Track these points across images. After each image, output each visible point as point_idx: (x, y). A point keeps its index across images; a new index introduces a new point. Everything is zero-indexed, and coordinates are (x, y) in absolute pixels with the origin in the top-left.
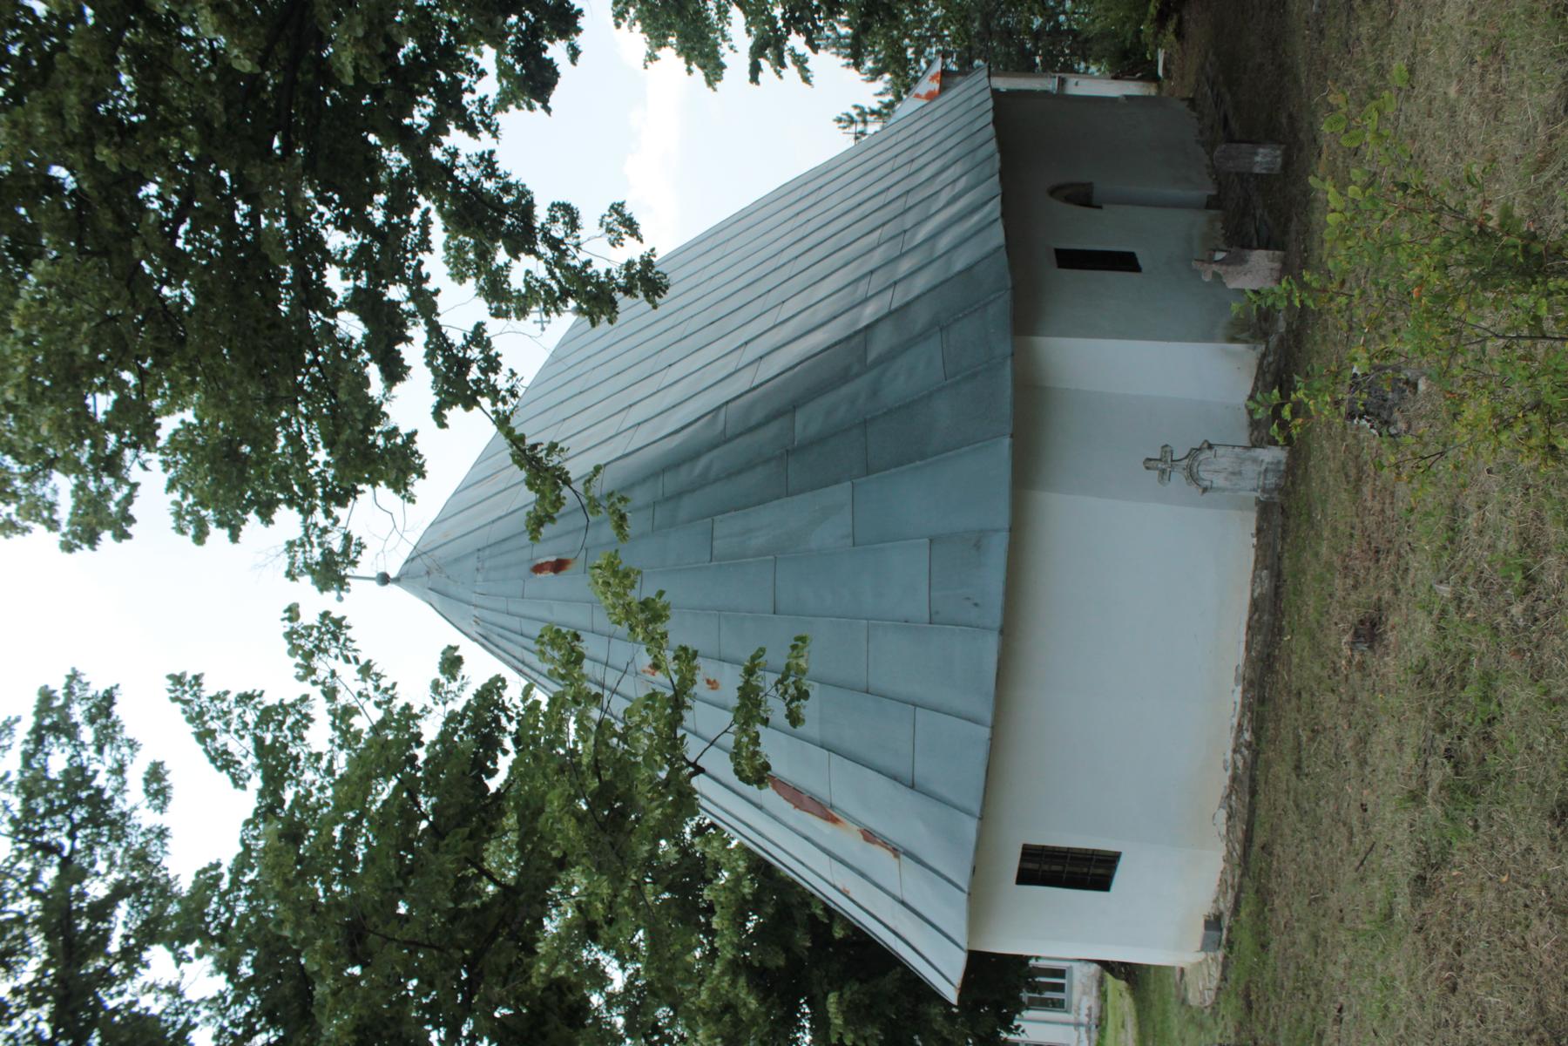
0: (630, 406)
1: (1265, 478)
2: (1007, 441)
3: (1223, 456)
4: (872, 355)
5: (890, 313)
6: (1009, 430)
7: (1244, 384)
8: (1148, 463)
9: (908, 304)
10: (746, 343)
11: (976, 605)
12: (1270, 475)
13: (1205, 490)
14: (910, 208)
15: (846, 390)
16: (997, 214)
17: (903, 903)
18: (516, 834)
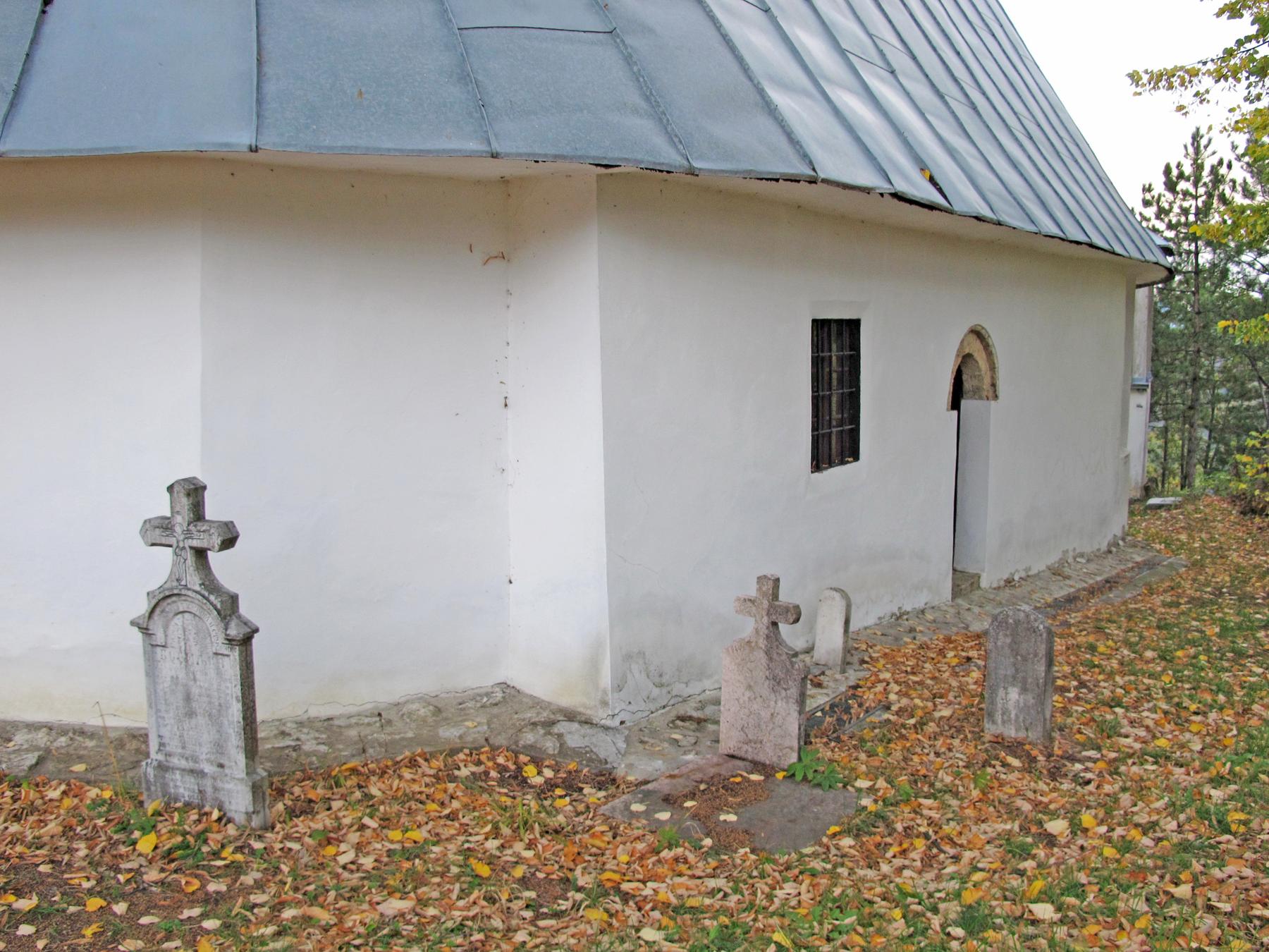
3: (219, 673)
8: (194, 492)
12: (191, 782)
13: (145, 631)
14: (946, 103)
18: (1010, 689)
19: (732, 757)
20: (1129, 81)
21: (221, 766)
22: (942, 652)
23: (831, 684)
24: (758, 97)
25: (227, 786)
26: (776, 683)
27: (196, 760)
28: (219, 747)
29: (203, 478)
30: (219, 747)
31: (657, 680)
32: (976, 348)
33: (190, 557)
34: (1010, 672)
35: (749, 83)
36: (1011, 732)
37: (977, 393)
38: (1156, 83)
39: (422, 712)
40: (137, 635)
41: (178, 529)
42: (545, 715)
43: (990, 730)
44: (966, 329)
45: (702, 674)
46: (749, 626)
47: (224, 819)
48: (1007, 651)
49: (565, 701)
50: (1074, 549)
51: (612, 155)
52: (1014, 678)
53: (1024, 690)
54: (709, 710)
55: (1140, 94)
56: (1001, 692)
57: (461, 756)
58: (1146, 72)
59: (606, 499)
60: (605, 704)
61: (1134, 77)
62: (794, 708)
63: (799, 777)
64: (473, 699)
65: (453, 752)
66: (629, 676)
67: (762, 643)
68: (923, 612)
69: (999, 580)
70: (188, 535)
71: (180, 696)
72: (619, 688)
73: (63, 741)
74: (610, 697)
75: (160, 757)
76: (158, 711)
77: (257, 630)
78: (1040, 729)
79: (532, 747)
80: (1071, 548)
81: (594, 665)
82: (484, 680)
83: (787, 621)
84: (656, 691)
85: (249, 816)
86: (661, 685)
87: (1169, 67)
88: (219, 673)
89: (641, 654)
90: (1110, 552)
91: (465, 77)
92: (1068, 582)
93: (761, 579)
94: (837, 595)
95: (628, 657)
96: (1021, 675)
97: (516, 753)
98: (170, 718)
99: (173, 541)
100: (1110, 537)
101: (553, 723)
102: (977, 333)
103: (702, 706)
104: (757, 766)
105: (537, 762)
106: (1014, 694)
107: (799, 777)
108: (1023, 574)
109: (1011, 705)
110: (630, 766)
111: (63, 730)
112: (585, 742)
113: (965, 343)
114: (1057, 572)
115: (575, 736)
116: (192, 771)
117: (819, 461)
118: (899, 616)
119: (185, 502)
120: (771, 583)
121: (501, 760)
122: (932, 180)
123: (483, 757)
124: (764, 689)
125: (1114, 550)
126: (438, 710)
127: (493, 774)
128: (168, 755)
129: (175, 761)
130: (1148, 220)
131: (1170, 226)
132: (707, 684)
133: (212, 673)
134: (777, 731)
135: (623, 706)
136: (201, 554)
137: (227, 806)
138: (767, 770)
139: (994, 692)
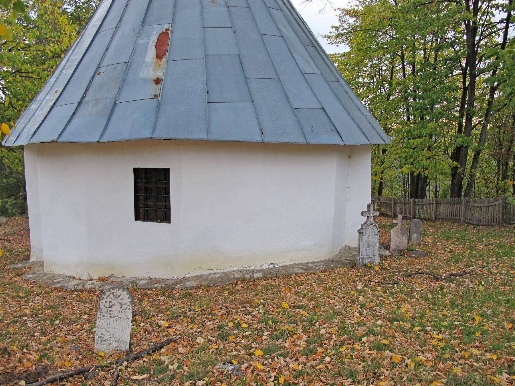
11: (312, 130)
12: (369, 260)
17: (115, 104)
26: (403, 234)
28: (373, 252)
30: (373, 252)
53: (417, 234)
56: (413, 235)
71: (367, 244)
75: (362, 257)
106: (416, 235)
116: (368, 258)
124: (400, 236)
133: (374, 238)
139: (412, 235)
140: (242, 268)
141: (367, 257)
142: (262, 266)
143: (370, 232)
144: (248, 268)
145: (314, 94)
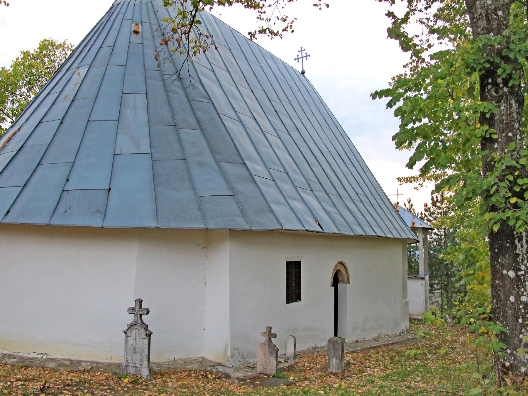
0: (229, 72)
1: (132, 367)
2: (154, 225)
3: (143, 343)
4: (225, 165)
5: (251, 174)
6: (160, 226)
7: (211, 356)
9: (255, 183)
10: (255, 119)
11: (66, 212)
12: (134, 369)
13: (126, 333)
14: (328, 195)
15: (207, 152)
16: (308, 228)
19: (260, 373)
20: (397, 181)
21: (142, 365)
22: (325, 356)
23: (290, 362)
24: (269, 209)
25: (143, 369)
26: (271, 353)
27: (135, 364)
28: (141, 360)
29: (142, 299)
30: (141, 360)
31: (242, 356)
32: (341, 268)
33: (139, 316)
34: (333, 354)
35: (267, 204)
36: (334, 371)
37: (343, 282)
38: (406, 181)
39: (181, 362)
40: (124, 334)
41: (136, 310)
42: (213, 364)
43: (329, 370)
44: (337, 262)
45: (254, 357)
46: (264, 339)
47: (141, 378)
48: (332, 349)
49: (218, 361)
50: (384, 333)
51: (234, 227)
52: (334, 356)
53: (337, 359)
54: (255, 366)
55: (401, 184)
56: (331, 360)
57: (192, 372)
58: (402, 178)
59: (230, 311)
60: (228, 361)
61: (399, 179)
62: (275, 359)
63: (276, 376)
64: (194, 360)
65: (191, 371)
66: (235, 355)
67: (267, 343)
68: (324, 348)
69: (352, 341)
70: (139, 311)
72: (232, 357)
73: (94, 365)
74: (230, 359)
75: (126, 364)
76: (127, 352)
77: (152, 333)
78: (341, 369)
79: (210, 370)
80: (382, 333)
81: (226, 351)
82: (197, 356)
83: (273, 337)
84: (242, 359)
85: (147, 376)
86: (243, 358)
87: (410, 176)
88: (143, 343)
89: (238, 349)
90: (400, 335)
91: (200, 209)
92: (378, 342)
93: (267, 327)
94: (292, 337)
95: (234, 349)
96: (336, 355)
97: (206, 372)
98: (130, 354)
99: (135, 313)
100: (400, 330)
101: (215, 366)
102: (341, 263)
103: (254, 365)
104: (265, 375)
105: (211, 374)
107: (276, 376)
108: (362, 340)
109: (334, 363)
110: (234, 375)
111: (94, 363)
112: (223, 370)
113: (337, 266)
114: (375, 340)
115: (220, 369)
116: (134, 367)
117: (289, 300)
118: (316, 348)
119: (138, 304)
120: (269, 328)
121: (202, 373)
122: (319, 224)
123: (198, 373)
124: (268, 355)
125: (402, 334)
126: (185, 363)
127: (200, 376)
128: (128, 363)
129: (130, 364)
130: (427, 216)
131: (435, 219)
132: (255, 359)
133: (141, 343)
134: (271, 365)
135: (233, 362)
136: (141, 315)
137: (142, 374)
138: (268, 376)
140: (11, 353)
141: (132, 365)
142: (29, 354)
143: (137, 334)
144: (16, 354)
145: (342, 184)
